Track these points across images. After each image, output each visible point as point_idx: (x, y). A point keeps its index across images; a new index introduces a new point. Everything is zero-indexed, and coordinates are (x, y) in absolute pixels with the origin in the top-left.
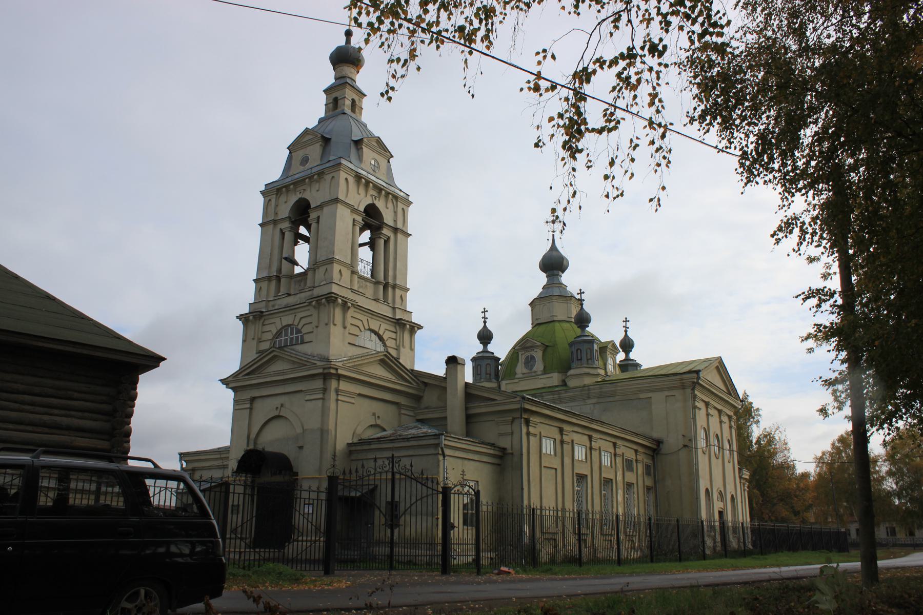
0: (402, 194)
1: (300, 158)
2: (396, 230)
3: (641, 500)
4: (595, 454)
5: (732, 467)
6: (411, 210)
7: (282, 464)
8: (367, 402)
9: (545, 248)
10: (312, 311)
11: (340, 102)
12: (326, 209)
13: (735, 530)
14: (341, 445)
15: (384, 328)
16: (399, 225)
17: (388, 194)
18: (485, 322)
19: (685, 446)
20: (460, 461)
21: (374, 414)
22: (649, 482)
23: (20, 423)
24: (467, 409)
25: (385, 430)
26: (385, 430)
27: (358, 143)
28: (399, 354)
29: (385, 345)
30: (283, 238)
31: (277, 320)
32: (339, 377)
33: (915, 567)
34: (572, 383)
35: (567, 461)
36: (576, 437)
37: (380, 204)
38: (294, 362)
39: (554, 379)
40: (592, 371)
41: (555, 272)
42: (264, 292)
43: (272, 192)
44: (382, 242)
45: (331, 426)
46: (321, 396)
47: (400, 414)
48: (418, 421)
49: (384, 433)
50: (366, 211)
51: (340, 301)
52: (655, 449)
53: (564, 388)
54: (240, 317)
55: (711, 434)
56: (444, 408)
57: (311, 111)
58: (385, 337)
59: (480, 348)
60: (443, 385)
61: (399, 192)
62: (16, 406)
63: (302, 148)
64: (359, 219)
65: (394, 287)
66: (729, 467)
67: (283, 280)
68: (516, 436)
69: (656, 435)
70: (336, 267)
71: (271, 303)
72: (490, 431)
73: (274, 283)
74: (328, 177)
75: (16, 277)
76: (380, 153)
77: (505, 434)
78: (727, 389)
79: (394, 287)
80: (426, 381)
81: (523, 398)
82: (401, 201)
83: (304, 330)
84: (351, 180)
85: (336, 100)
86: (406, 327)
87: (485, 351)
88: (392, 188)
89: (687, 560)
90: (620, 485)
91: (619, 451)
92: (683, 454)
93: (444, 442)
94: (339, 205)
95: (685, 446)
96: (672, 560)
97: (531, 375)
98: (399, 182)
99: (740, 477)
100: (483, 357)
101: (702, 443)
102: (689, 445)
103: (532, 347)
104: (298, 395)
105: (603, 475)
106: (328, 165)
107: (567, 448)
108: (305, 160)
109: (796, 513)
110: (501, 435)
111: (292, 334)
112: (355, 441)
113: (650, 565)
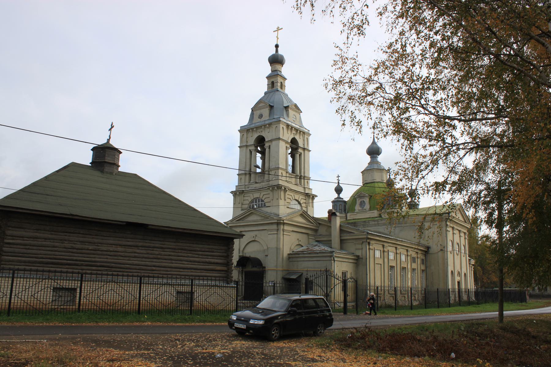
0: (306, 131)
1: (258, 115)
2: (304, 149)
3: (419, 276)
4: (398, 256)
5: (465, 259)
6: (311, 138)
7: (257, 262)
8: (295, 234)
9: (369, 143)
10: (269, 192)
11: (275, 84)
12: (274, 142)
14: (285, 255)
15: (301, 198)
16: (306, 147)
17: (300, 131)
19: (441, 250)
20: (340, 263)
21: (298, 239)
22: (423, 267)
23: (195, 262)
24: (340, 237)
26: (302, 246)
27: (287, 108)
28: (307, 210)
29: (301, 206)
30: (251, 154)
31: (251, 195)
32: (284, 224)
33: (539, 314)
35: (386, 260)
36: (390, 248)
37: (297, 137)
38: (262, 216)
39: (375, 213)
41: (375, 155)
42: (243, 181)
43: (244, 131)
44: (298, 155)
45: (281, 246)
47: (309, 238)
48: (317, 241)
49: (303, 248)
50: (291, 142)
52: (426, 251)
53: (380, 218)
54: (232, 192)
56: (330, 235)
60: (329, 225)
62: (197, 256)
64: (288, 146)
66: (464, 259)
67: (252, 175)
72: (351, 247)
74: (274, 126)
75: (180, 201)
76: (296, 111)
77: (359, 249)
78: (464, 219)
80: (320, 222)
81: (368, 233)
82: (305, 134)
83: (265, 201)
84: (285, 127)
85: (273, 83)
87: (339, 198)
88: (302, 129)
89: (443, 307)
90: (410, 270)
91: (409, 254)
92: (440, 254)
93: (335, 255)
95: (441, 250)
96: (434, 307)
97: (363, 211)
98: (305, 125)
99: (470, 264)
100: (338, 201)
101: (450, 248)
102: (443, 250)
103: (364, 197)
104: (263, 231)
105: (402, 266)
106: (274, 120)
107: (386, 254)
108: (261, 116)
110: (356, 249)
111: (259, 202)
112: (291, 252)
113: (425, 310)
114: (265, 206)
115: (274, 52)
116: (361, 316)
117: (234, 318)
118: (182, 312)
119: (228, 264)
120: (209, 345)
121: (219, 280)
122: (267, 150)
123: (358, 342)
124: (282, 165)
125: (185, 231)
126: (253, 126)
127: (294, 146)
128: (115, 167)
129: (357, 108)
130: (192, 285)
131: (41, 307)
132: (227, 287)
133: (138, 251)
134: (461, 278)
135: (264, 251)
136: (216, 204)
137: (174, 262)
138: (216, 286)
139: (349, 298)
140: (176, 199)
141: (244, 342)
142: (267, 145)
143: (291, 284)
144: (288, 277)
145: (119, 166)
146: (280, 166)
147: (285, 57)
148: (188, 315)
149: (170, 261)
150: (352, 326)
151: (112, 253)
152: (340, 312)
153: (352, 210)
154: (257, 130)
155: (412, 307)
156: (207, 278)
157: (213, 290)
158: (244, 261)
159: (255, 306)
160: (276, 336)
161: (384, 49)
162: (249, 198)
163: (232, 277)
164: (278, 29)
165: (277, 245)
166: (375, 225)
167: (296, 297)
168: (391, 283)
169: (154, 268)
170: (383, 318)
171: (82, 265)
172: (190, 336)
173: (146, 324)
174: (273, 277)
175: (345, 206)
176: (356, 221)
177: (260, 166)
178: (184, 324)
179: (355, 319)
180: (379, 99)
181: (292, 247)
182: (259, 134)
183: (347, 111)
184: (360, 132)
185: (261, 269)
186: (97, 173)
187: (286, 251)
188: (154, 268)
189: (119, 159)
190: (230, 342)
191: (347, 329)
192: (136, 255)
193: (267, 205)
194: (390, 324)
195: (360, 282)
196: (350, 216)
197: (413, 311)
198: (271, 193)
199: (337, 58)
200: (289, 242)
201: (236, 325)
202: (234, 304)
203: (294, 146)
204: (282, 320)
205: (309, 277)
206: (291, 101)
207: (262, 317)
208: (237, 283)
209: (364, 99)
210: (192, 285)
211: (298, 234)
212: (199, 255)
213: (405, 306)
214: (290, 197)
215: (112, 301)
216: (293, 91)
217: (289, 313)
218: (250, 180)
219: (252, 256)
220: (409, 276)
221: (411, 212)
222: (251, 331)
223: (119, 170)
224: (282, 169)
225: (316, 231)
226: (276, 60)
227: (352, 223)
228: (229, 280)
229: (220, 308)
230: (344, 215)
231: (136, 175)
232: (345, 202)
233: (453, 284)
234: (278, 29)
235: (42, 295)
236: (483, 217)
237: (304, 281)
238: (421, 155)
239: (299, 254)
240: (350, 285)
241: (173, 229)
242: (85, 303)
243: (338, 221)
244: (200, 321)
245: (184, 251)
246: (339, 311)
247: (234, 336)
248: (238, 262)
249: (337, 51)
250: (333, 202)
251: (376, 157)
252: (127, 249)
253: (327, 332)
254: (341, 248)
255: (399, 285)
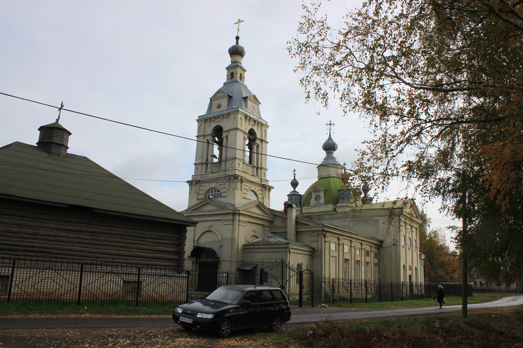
0: (264, 122)
1: (216, 105)
2: (262, 141)
3: (373, 270)
5: (416, 253)
6: (268, 130)
7: (211, 253)
9: (325, 139)
11: (234, 75)
12: (231, 133)
13: (416, 285)
14: (240, 246)
15: (257, 189)
16: (263, 138)
17: (258, 123)
18: (295, 176)
19: (394, 244)
21: (254, 231)
22: (376, 261)
23: (144, 249)
24: (296, 229)
25: (258, 238)
26: (258, 238)
27: (245, 98)
28: (263, 201)
29: (257, 197)
31: (207, 185)
32: (240, 214)
33: (492, 308)
34: (339, 210)
35: (341, 253)
36: (345, 241)
37: (255, 128)
39: (330, 207)
40: (349, 205)
41: (331, 151)
43: (202, 120)
44: (255, 146)
45: (236, 237)
46: (231, 223)
47: (264, 230)
48: (272, 233)
49: (258, 239)
51: (240, 178)
52: (380, 245)
53: (335, 212)
55: (407, 238)
56: (286, 227)
57: (220, 79)
58: (258, 193)
59: (292, 189)
60: (285, 216)
61: (263, 121)
63: (218, 99)
64: (246, 137)
65: (261, 168)
66: (415, 253)
67: (209, 165)
68: (319, 242)
69: (380, 238)
70: (237, 161)
71: (203, 176)
72: (307, 239)
73: (204, 166)
74: (232, 117)
75: (131, 186)
76: (255, 103)
79: (261, 168)
80: (276, 214)
81: (324, 225)
82: (263, 125)
83: (221, 191)
84: (243, 118)
85: (232, 74)
86: (266, 188)
87: (294, 191)
88: (260, 120)
89: (396, 300)
90: (363, 263)
91: (363, 247)
92: (393, 248)
93: (290, 246)
94: (239, 132)
95: (394, 244)
96: (388, 300)
97: (318, 205)
98: (263, 117)
99: (420, 258)
100: (293, 195)
101: (402, 243)
102: (396, 244)
103: (319, 191)
105: (356, 259)
106: (232, 110)
107: (341, 247)
108: (219, 106)
109: (448, 274)
110: (312, 241)
111: (215, 192)
112: (246, 243)
113: (379, 303)
114: (221, 196)
115: (234, 44)
116: (317, 309)
117: (180, 311)
118: (128, 303)
119: (180, 252)
120: (147, 343)
121: (169, 269)
122: (225, 140)
123: (321, 340)
124: (239, 155)
125: (134, 216)
126: (211, 115)
127: (252, 137)
128: (63, 148)
129: (323, 80)
130: (139, 274)
131: (41, 297)
132: (177, 277)
133: (82, 236)
134: (412, 273)
135: (219, 241)
136: (176, 198)
137: (121, 249)
138: (165, 275)
139: (304, 291)
140: (127, 184)
141: (189, 340)
142: (224, 135)
143: (245, 275)
144: (242, 268)
145: (68, 148)
146: (237, 156)
147: (246, 49)
148: (134, 306)
149: (117, 248)
150: (312, 320)
151: (53, 238)
152: (294, 304)
153: (308, 203)
154: (215, 120)
155: (366, 300)
156: (156, 267)
157: (162, 280)
158: (198, 251)
159: (204, 298)
160: (226, 332)
161: (354, 16)
162: (206, 187)
163: (184, 267)
164: (240, 21)
165: (232, 236)
166: (330, 219)
167: (251, 288)
168: (345, 276)
169: (99, 255)
170: (340, 312)
171: (18, 250)
172: (128, 331)
173: (83, 316)
174: (227, 267)
175: (300, 200)
176: (311, 214)
177: (218, 157)
178: (127, 316)
179: (311, 313)
180: (347, 69)
181: (248, 238)
182: (217, 124)
183: (312, 82)
184: (326, 105)
185: (215, 260)
186: (44, 154)
187: (241, 242)
188: (99, 255)
189: (68, 140)
190: (173, 338)
191: (305, 323)
192: (80, 240)
193: (223, 195)
194: (350, 318)
195: (315, 275)
196: (305, 210)
197: (368, 305)
198: (228, 184)
199: (303, 21)
200: (244, 233)
201: (182, 319)
202: (184, 295)
203: (252, 137)
204: (234, 313)
205: (264, 268)
206: (249, 92)
207: (212, 310)
208: (188, 272)
209: (330, 69)
210: (139, 274)
211: (254, 225)
212: (149, 242)
213: (359, 299)
214: (247, 188)
215: (48, 290)
216: (252, 82)
217: (242, 305)
218: (207, 170)
219: (207, 246)
220: (363, 269)
221: (366, 207)
222: (198, 326)
223: (68, 152)
224: (239, 159)
225: (272, 222)
226: (236, 52)
227: (307, 217)
228: (180, 269)
229: (170, 298)
230: (299, 209)
231: (86, 158)
232: (301, 196)
233: (405, 278)
234: (240, 21)
235: (43, 285)
236: (450, 206)
237: (259, 272)
238: (390, 135)
239: (254, 245)
240: (305, 276)
241: (121, 214)
242: (32, 292)
243: (294, 213)
244: (146, 313)
245: (132, 238)
246: (293, 303)
247: (179, 331)
248: (192, 252)
249: (304, 12)
250: (289, 195)
251: (332, 153)
252: (70, 234)
253: (283, 328)
254: (297, 240)
255: (353, 278)
